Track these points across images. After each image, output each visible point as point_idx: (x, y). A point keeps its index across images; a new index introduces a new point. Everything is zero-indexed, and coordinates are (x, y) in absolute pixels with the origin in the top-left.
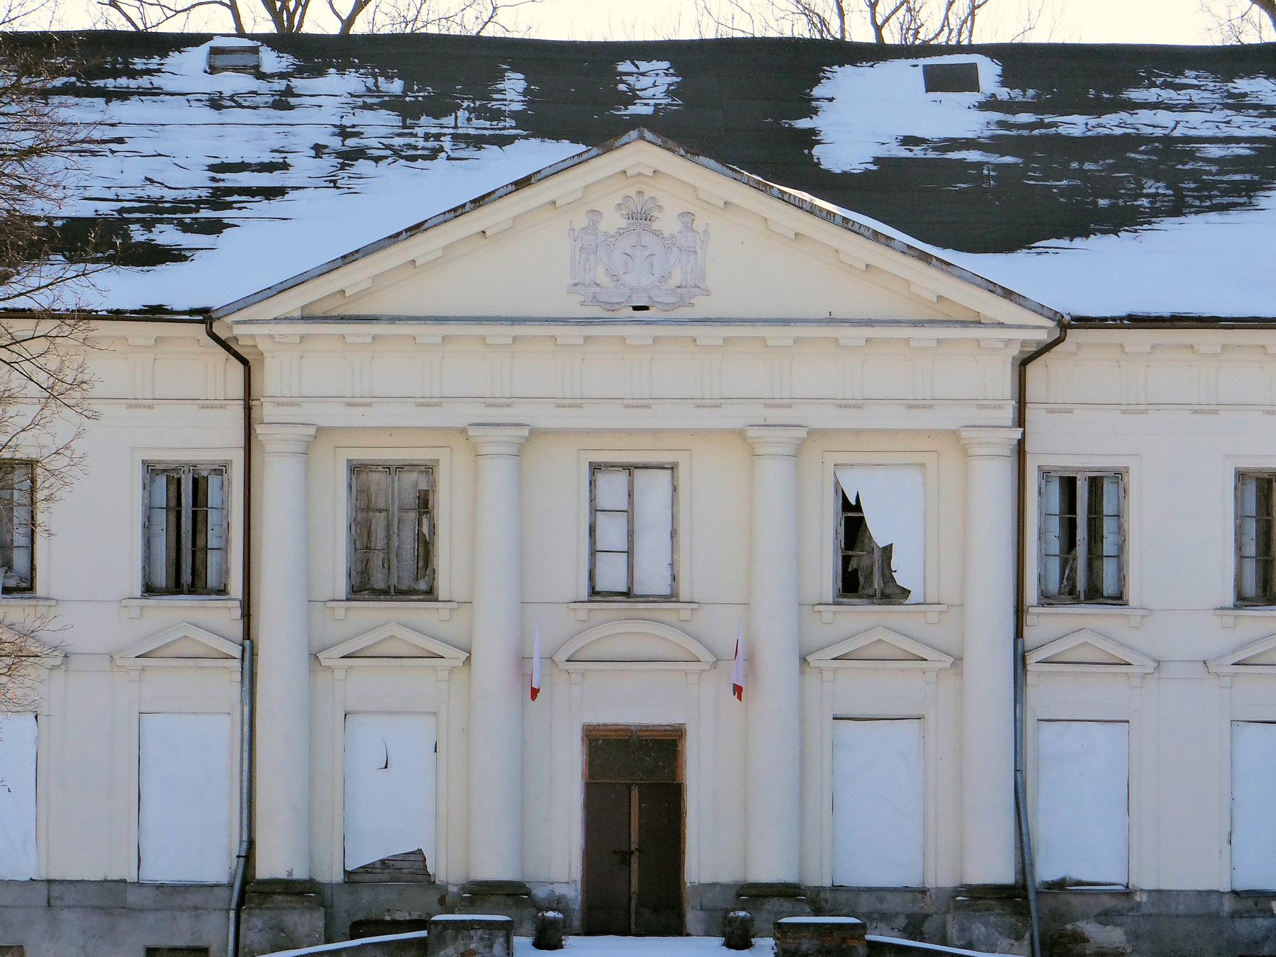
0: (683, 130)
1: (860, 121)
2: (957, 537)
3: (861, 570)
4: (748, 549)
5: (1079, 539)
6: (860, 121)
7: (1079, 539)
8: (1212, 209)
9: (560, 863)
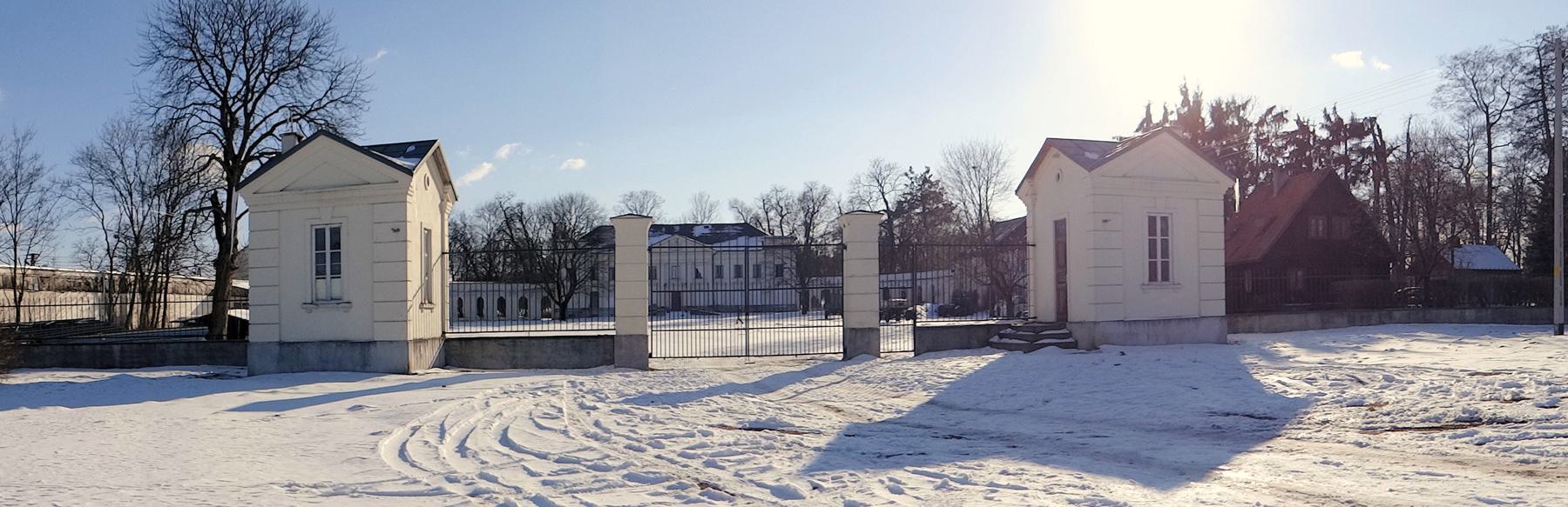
0: (680, 233)
1: (697, 232)
2: (708, 273)
3: (698, 275)
4: (687, 275)
5: (719, 271)
6: (697, 232)
7: (719, 271)
8: (718, 234)
9: (668, 304)
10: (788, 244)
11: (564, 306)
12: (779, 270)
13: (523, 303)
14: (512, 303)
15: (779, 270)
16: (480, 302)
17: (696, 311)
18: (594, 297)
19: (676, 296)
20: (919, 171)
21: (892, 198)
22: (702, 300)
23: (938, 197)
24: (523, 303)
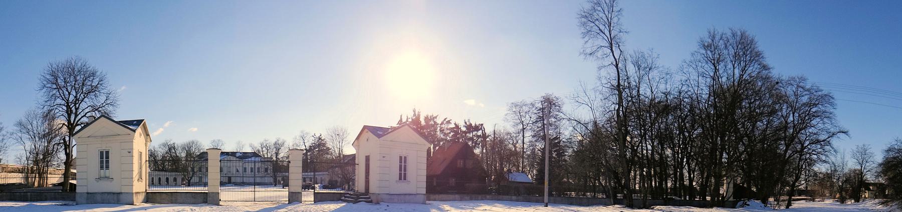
2: (241, 169)
6: (238, 155)
8: (245, 156)
10: (269, 160)
11: (189, 181)
12: (266, 170)
13: (175, 180)
14: (171, 179)
15: (266, 170)
16: (167, 179)
17: (236, 184)
18: (201, 178)
19: (230, 178)
20: (318, 135)
21: (308, 145)
22: (239, 180)
23: (324, 145)
24: (175, 180)
